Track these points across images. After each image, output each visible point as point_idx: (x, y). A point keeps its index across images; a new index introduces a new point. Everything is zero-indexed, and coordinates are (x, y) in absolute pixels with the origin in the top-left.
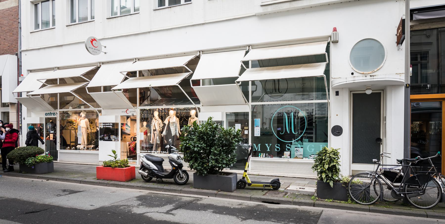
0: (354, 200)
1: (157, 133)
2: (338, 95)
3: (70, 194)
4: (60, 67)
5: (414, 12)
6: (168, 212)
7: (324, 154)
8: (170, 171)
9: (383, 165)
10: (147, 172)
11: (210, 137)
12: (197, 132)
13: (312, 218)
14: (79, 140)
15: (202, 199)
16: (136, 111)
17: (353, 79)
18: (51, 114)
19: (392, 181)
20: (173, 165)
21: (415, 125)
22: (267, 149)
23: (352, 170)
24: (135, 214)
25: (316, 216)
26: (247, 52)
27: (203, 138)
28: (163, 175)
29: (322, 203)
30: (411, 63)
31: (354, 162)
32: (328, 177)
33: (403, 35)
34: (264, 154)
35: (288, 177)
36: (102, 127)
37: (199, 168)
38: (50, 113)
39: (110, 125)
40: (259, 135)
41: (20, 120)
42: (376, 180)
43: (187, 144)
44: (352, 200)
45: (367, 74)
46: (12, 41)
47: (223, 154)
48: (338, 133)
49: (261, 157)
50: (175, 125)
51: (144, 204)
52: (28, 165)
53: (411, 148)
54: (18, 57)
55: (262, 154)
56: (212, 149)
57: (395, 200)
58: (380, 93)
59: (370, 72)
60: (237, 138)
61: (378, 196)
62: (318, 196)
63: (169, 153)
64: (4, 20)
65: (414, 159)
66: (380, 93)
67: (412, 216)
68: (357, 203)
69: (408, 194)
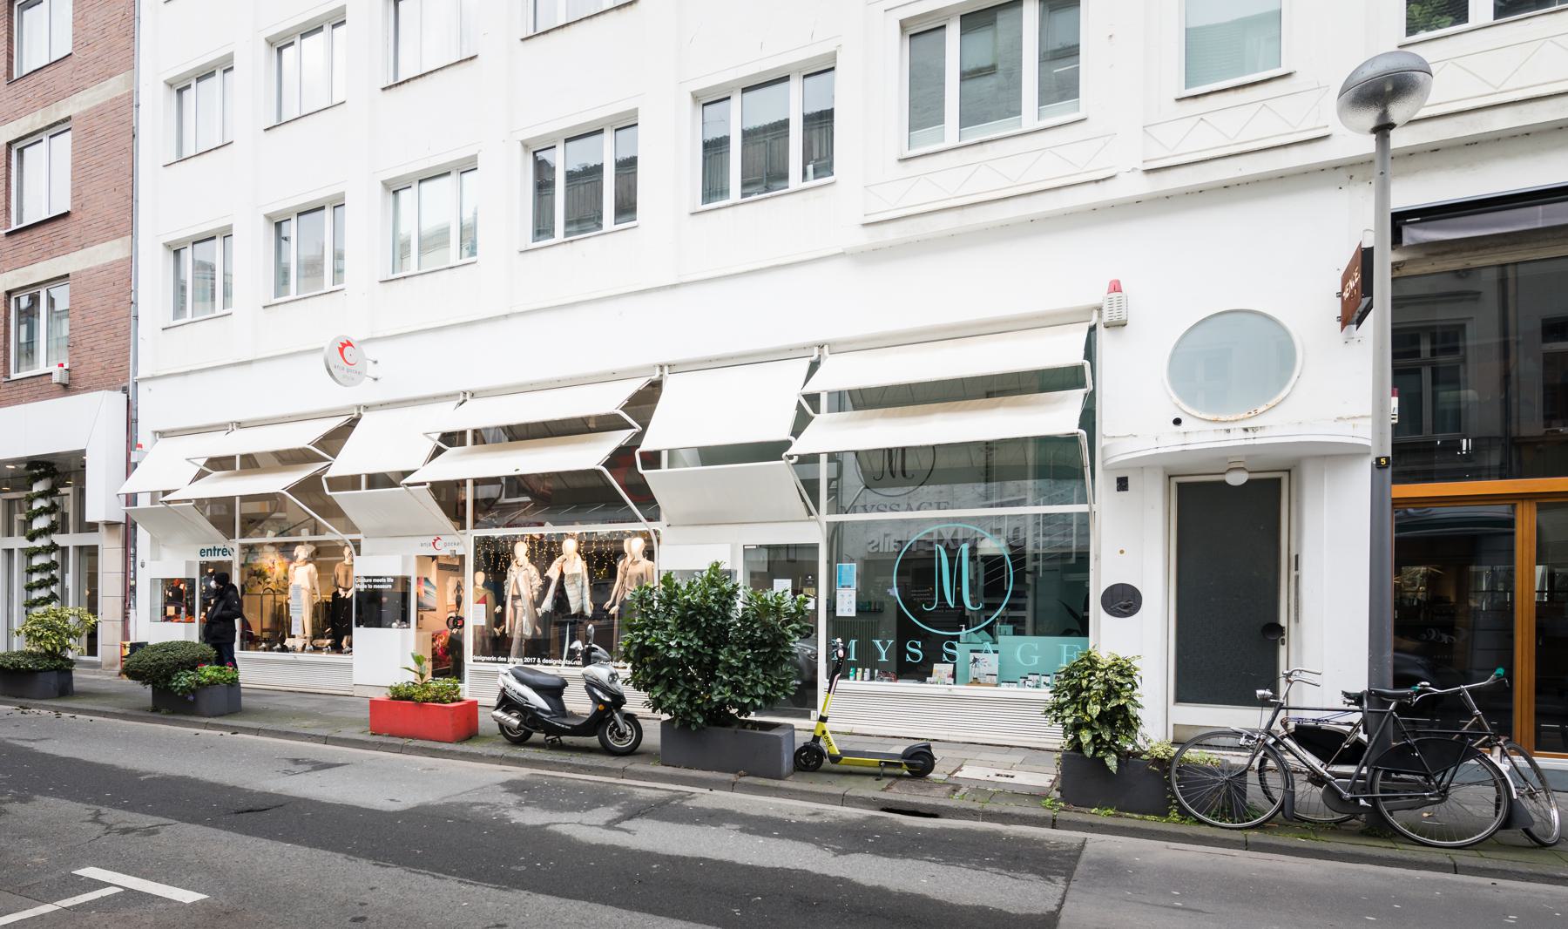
0: (1190, 814)
1: (524, 605)
2: (1127, 490)
3: (315, 769)
4: (245, 422)
5: (1408, 220)
6: (610, 825)
7: (1086, 672)
8: (588, 717)
9: (1287, 709)
10: (517, 717)
11: (716, 618)
12: (676, 604)
13: (1054, 858)
14: (296, 620)
15: (693, 795)
16: (464, 543)
17: (1182, 440)
18: (215, 551)
19: (1325, 758)
20: (599, 698)
21: (1409, 580)
22: (879, 655)
23: (1175, 725)
24: (519, 828)
25: (1066, 854)
26: (814, 367)
27: (694, 623)
28: (568, 725)
29: (1080, 817)
30: (1394, 385)
31: (1181, 698)
32: (1099, 741)
33: (1363, 297)
34: (867, 670)
35: (948, 742)
36: (362, 588)
37: (681, 708)
38: (215, 549)
39: (387, 583)
40: (853, 614)
41: (132, 569)
42: (1268, 752)
43: (645, 638)
44: (1184, 813)
45: (1231, 421)
46: (112, 353)
47: (756, 668)
48: (1126, 607)
49: (855, 679)
50: (579, 583)
51: (534, 804)
52: (178, 691)
53: (1395, 657)
54: (128, 396)
55: (860, 670)
56: (720, 654)
57: (1338, 817)
58: (1278, 481)
59: (1241, 416)
60: (797, 623)
61: (1274, 804)
62: (1065, 797)
63: (584, 665)
64: (90, 298)
65: (1408, 691)
66: (1278, 481)
67: (1398, 866)
68: (1201, 822)
69: (1384, 799)
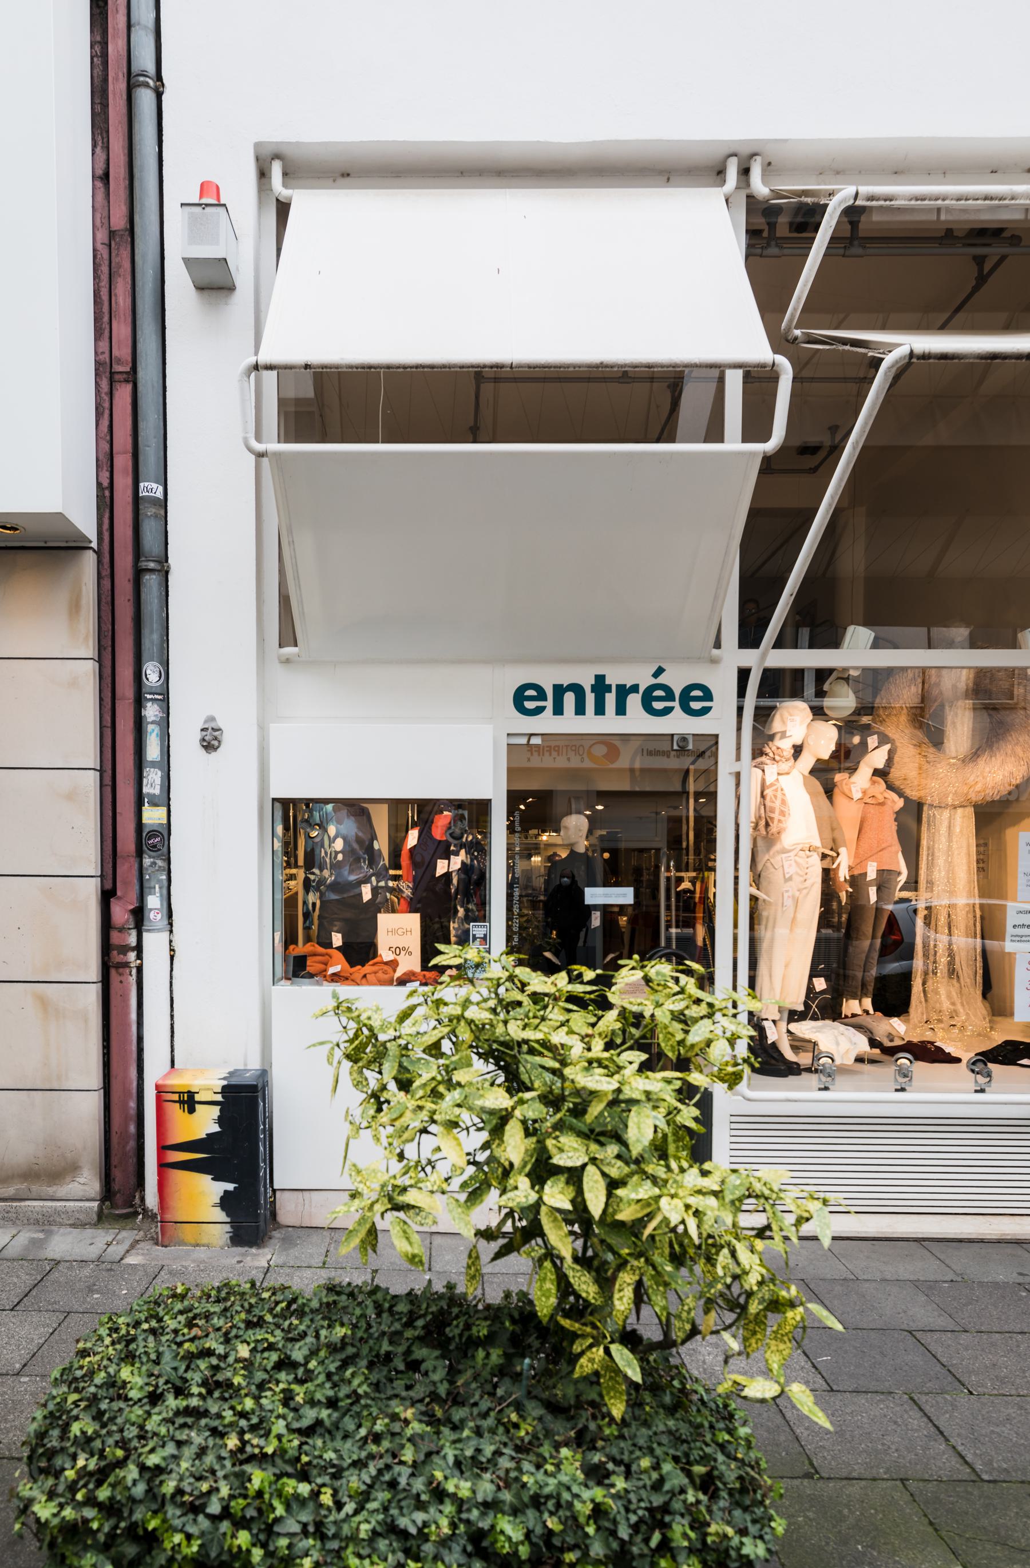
38: (600, 686)
